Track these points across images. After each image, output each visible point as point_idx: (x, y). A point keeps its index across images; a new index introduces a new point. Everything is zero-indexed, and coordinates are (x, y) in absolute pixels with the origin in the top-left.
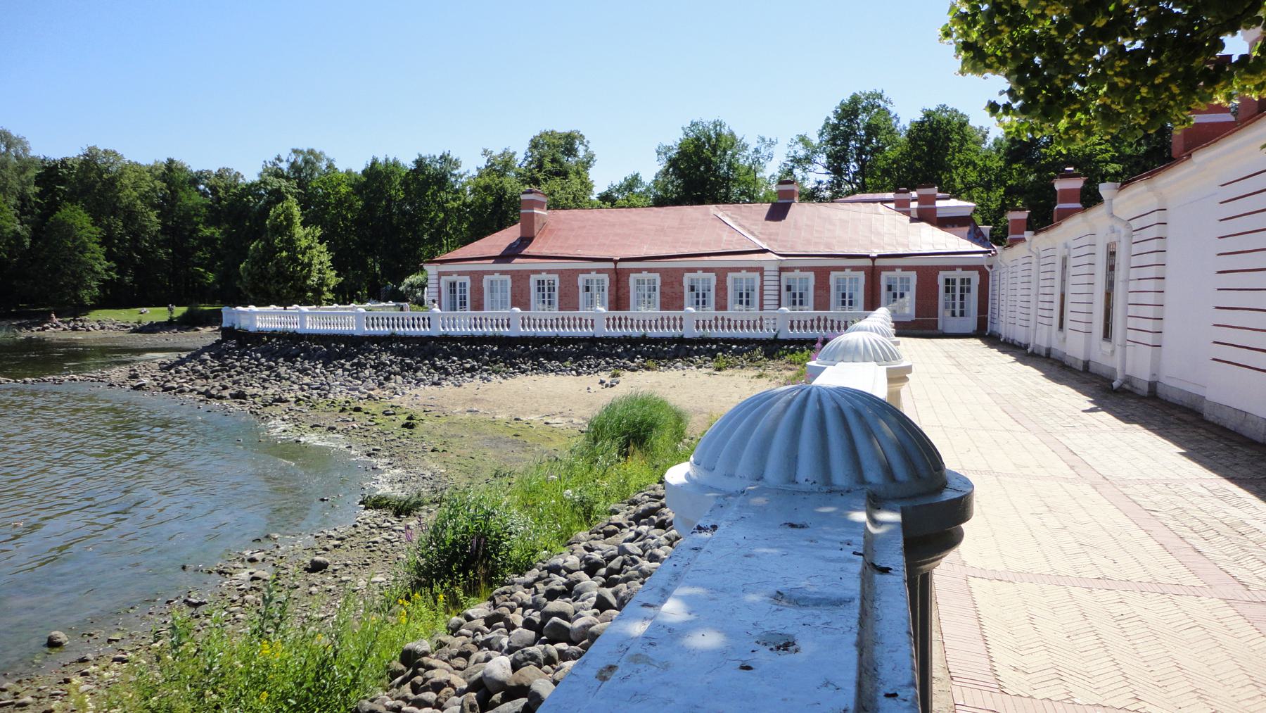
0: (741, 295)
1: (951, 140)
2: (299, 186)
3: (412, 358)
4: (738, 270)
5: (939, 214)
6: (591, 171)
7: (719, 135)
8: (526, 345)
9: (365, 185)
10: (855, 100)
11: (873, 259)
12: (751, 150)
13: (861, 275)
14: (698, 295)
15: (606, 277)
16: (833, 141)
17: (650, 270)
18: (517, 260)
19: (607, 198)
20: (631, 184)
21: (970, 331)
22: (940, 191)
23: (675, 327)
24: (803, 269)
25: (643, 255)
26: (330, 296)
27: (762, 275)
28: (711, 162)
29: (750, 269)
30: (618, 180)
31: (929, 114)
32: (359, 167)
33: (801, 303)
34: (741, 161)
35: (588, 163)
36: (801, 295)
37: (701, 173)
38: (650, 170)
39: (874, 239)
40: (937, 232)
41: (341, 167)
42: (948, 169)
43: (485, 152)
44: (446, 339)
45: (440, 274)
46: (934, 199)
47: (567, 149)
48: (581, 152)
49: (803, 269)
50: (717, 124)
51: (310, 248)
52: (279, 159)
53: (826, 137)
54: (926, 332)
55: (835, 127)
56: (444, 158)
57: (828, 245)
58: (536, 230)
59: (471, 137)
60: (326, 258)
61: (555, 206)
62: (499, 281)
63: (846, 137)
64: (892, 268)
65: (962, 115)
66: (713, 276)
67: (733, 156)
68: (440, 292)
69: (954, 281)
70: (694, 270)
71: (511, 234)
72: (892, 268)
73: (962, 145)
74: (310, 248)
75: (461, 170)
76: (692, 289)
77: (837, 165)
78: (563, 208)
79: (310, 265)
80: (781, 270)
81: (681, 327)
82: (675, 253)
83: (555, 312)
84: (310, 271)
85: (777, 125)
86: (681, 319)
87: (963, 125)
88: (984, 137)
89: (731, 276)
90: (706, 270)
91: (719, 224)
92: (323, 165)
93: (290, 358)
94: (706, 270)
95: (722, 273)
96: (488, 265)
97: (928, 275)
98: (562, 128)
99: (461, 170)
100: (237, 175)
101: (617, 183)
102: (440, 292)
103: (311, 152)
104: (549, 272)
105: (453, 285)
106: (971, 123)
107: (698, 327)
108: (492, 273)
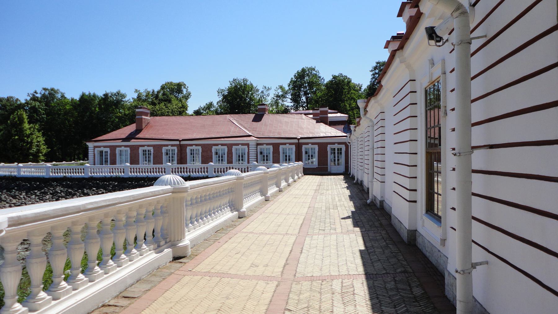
0: (239, 156)
1: (344, 89)
2: (46, 105)
3: (72, 189)
4: (237, 145)
5: (329, 120)
6: (189, 100)
7: (245, 85)
8: (132, 182)
9: (79, 105)
10: (303, 70)
11: (299, 139)
12: (260, 91)
13: (294, 147)
14: (219, 157)
15: (175, 148)
16: (294, 89)
17: (196, 145)
18: (133, 140)
19: (198, 113)
20: (210, 105)
21: (342, 172)
22: (330, 109)
23: (204, 172)
24: (267, 144)
25: (193, 137)
26: (42, 158)
27: (248, 147)
28: (242, 97)
29: (243, 144)
30: (203, 105)
31: (335, 77)
32: (77, 97)
33: (267, 160)
34: (255, 97)
35: (187, 97)
36: (267, 156)
37: (238, 100)
38: (216, 99)
39: (300, 130)
40: (328, 127)
41: (69, 96)
42: (343, 101)
43: (136, 91)
44: (92, 179)
45: (95, 147)
46: (327, 113)
47: (178, 90)
48: (185, 91)
49: (267, 144)
50: (245, 80)
51: (31, 134)
52: (36, 92)
53: (291, 86)
54: (323, 173)
55: (295, 82)
56: (118, 93)
57: (279, 133)
58: (144, 126)
59: (130, 83)
60: (41, 139)
61: (153, 114)
62: (124, 151)
63: (300, 86)
64: (307, 144)
65: (349, 78)
66: (226, 148)
67: (252, 94)
68: (94, 156)
69: (334, 149)
70: (217, 145)
71: (132, 128)
72: (307, 144)
73: (349, 91)
74: (31, 134)
75: (126, 99)
76: (217, 153)
77: (296, 99)
78: (167, 116)
79: (31, 143)
80: (258, 144)
81: (207, 172)
82: (209, 137)
83: (152, 165)
84: (31, 146)
85: (270, 80)
86: (207, 168)
87: (349, 82)
88: (360, 88)
89: (234, 147)
90: (222, 145)
91: (230, 123)
92: (59, 96)
93: (9, 190)
94: (222, 145)
95: (230, 146)
96: (119, 143)
97: (323, 146)
98: (176, 81)
99: (126, 99)
100: (17, 100)
101: (202, 106)
102: (94, 156)
103: (52, 89)
104: (148, 146)
105: (101, 152)
106: (352, 82)
107: (215, 172)
108: (120, 146)
